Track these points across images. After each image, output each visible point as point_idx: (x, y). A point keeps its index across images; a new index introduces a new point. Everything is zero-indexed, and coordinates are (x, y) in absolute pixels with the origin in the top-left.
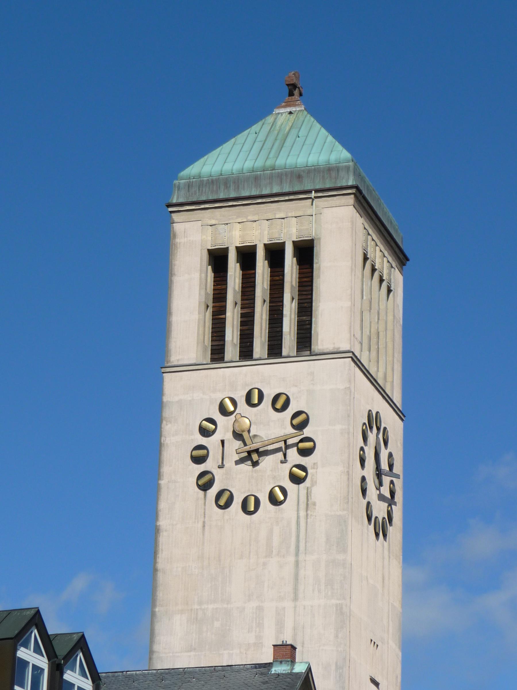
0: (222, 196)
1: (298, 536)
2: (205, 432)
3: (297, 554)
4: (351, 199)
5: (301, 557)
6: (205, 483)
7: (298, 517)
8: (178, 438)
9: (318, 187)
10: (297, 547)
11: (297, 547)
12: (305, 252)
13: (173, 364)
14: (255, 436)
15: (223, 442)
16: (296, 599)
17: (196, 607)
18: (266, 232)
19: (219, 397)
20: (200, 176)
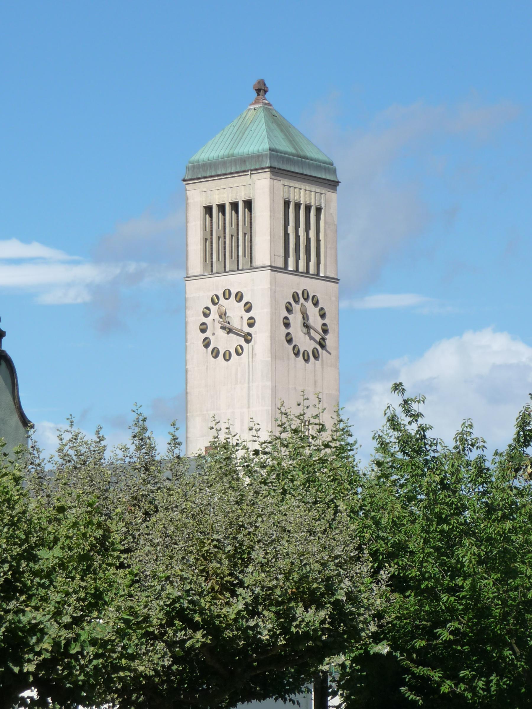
0: (208, 175)
1: (249, 373)
2: (206, 315)
3: (249, 383)
4: (268, 175)
5: (250, 385)
6: (207, 343)
7: (249, 362)
8: (195, 318)
9: (252, 168)
10: (249, 379)
11: (249, 379)
12: (248, 204)
13: (191, 275)
14: (228, 316)
15: (214, 320)
16: (249, 407)
17: (205, 413)
18: (230, 196)
19: (212, 294)
20: (198, 161)
